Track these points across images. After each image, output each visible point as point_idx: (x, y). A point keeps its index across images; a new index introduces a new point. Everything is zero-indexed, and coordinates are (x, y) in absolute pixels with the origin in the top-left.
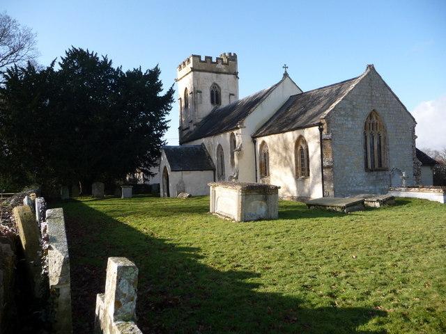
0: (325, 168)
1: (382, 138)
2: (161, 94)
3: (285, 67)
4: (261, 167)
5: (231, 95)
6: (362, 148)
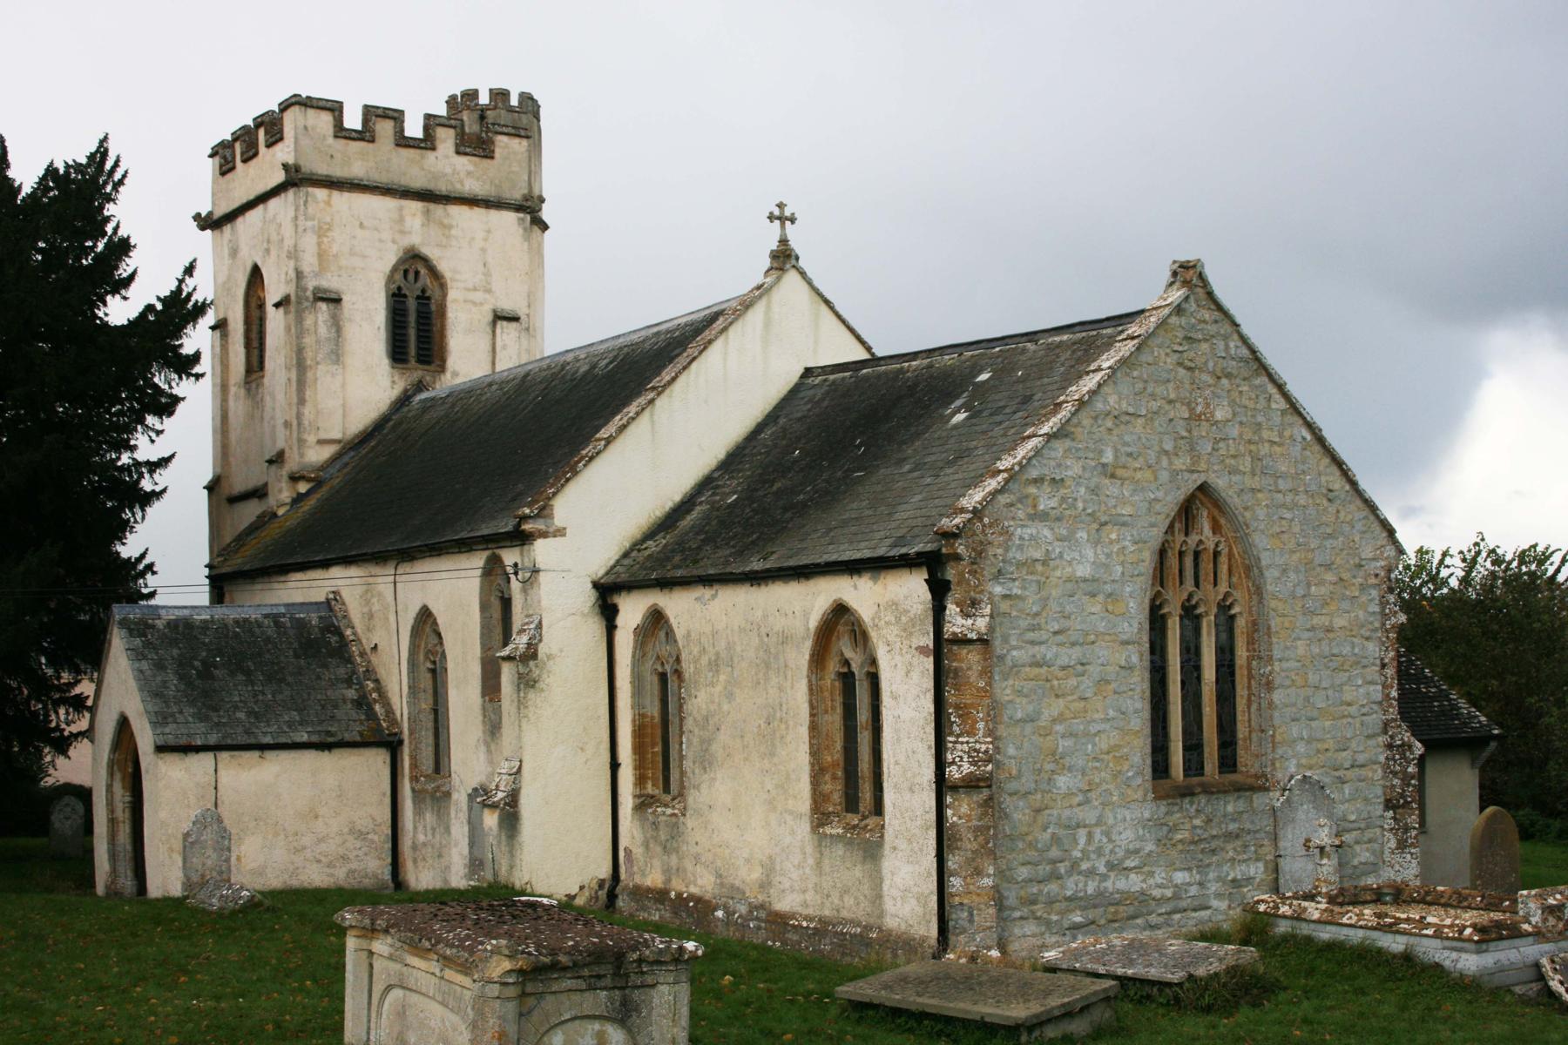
0: (955, 788)
1: (1241, 624)
2: (118, 311)
3: (782, 217)
4: (639, 748)
5: (499, 317)
6: (1140, 682)
